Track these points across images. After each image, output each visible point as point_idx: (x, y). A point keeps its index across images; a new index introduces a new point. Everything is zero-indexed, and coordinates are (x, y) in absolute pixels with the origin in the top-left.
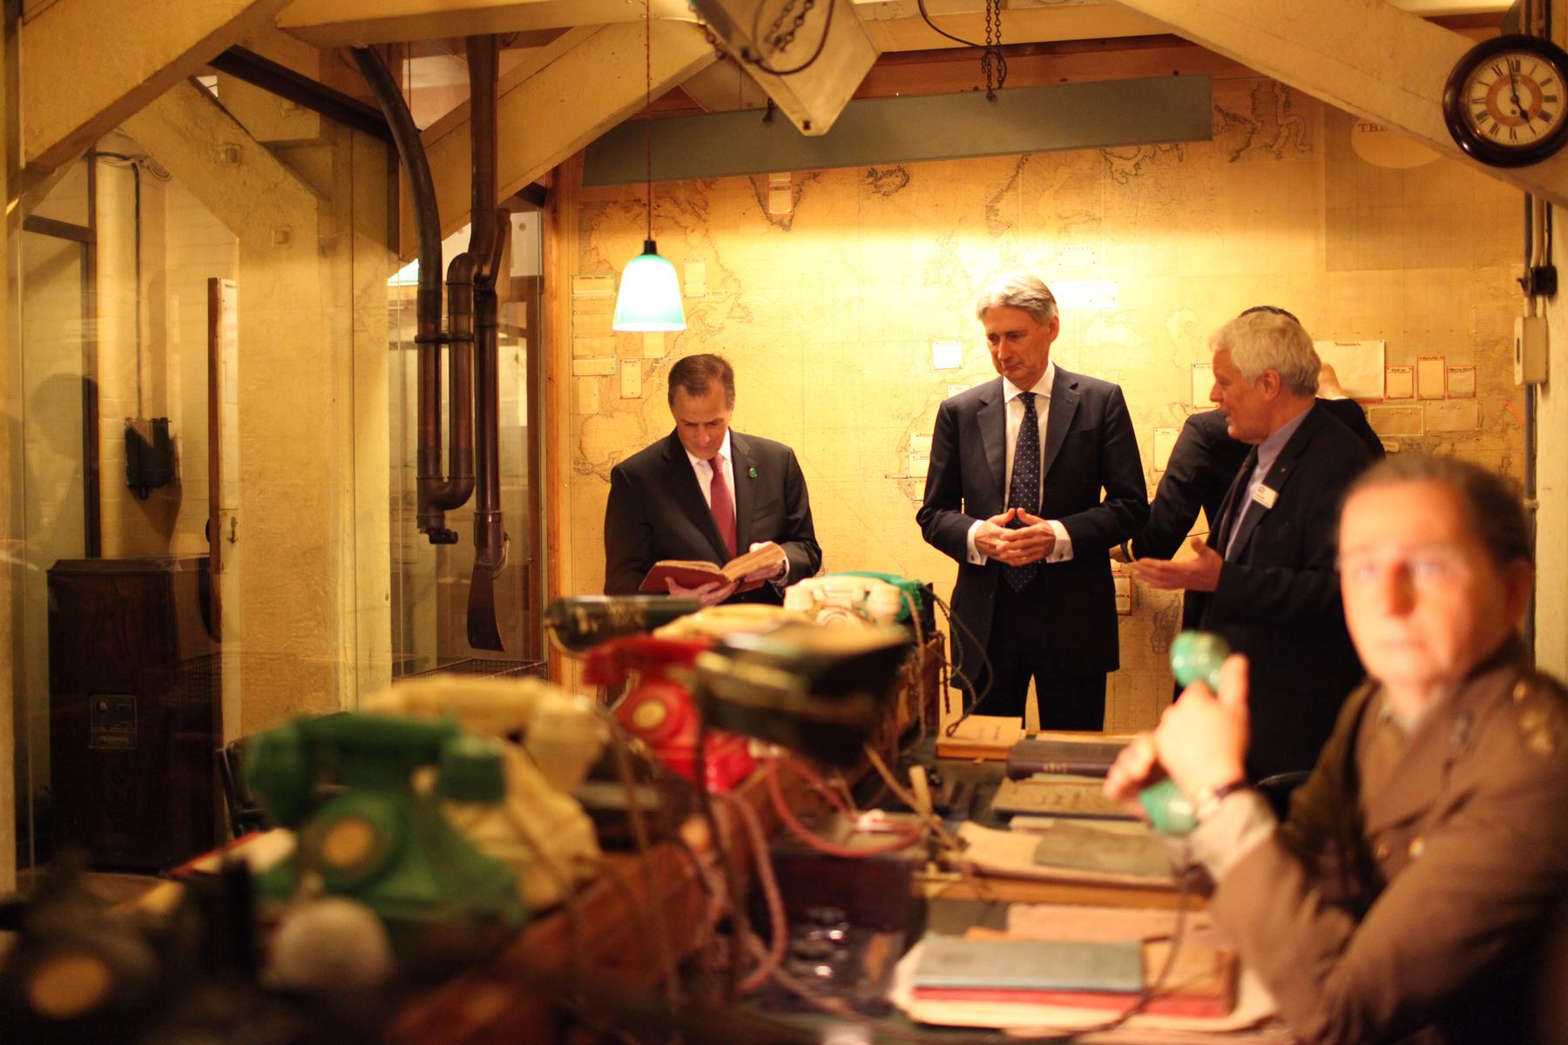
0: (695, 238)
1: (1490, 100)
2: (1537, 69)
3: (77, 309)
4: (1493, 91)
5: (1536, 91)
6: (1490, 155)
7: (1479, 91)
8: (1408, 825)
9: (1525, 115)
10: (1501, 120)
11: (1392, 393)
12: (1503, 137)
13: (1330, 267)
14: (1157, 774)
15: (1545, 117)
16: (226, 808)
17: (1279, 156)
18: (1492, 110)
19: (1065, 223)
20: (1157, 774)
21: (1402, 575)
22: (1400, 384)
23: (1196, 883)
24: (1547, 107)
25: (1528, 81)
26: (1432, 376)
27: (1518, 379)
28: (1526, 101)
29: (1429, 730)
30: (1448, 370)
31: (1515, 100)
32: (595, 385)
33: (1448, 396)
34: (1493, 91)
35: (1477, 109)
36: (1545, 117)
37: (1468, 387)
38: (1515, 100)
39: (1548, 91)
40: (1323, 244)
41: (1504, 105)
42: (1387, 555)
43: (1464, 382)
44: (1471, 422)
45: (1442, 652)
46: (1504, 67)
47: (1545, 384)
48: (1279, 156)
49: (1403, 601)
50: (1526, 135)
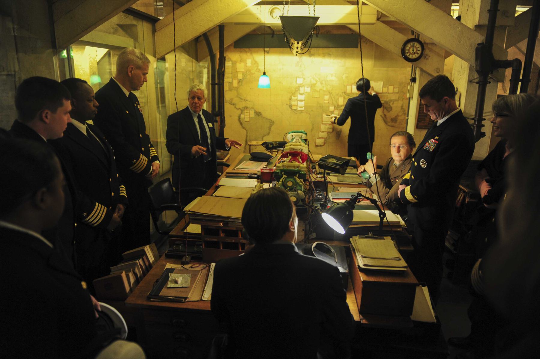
0: (249, 54)
1: (409, 50)
2: (417, 45)
3: (107, 63)
4: (410, 48)
5: (417, 49)
6: (407, 59)
7: (407, 48)
8: (396, 178)
9: (414, 53)
10: (411, 54)
11: (384, 91)
12: (410, 57)
13: (374, 66)
14: (365, 171)
15: (418, 54)
16: (463, 188)
17: (366, 44)
18: (409, 52)
19: (324, 55)
20: (365, 171)
21: (399, 147)
22: (385, 90)
23: (368, 185)
24: (418, 52)
25: (415, 47)
26: (391, 89)
27: (408, 96)
28: (415, 51)
29: (400, 166)
30: (394, 88)
31: (413, 50)
32: (228, 84)
33: (393, 93)
34: (410, 48)
35: (407, 51)
36: (418, 54)
37: (397, 91)
38: (413, 50)
39: (418, 49)
40: (373, 62)
41: (411, 51)
42: (397, 145)
43: (397, 90)
44: (397, 98)
45: (403, 157)
46: (412, 44)
47: (412, 98)
48: (366, 44)
49: (399, 151)
50: (414, 57)
